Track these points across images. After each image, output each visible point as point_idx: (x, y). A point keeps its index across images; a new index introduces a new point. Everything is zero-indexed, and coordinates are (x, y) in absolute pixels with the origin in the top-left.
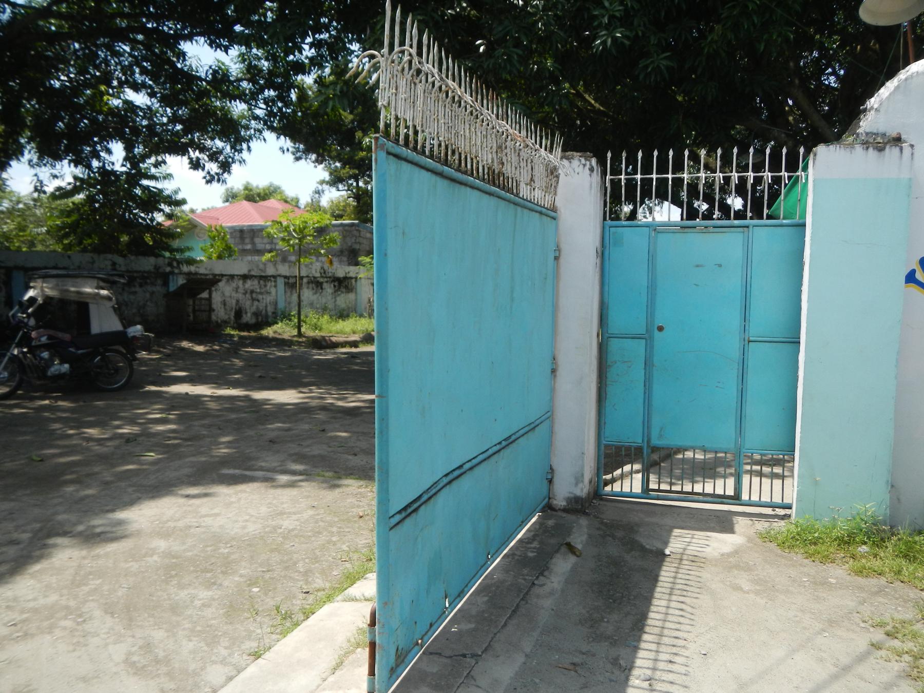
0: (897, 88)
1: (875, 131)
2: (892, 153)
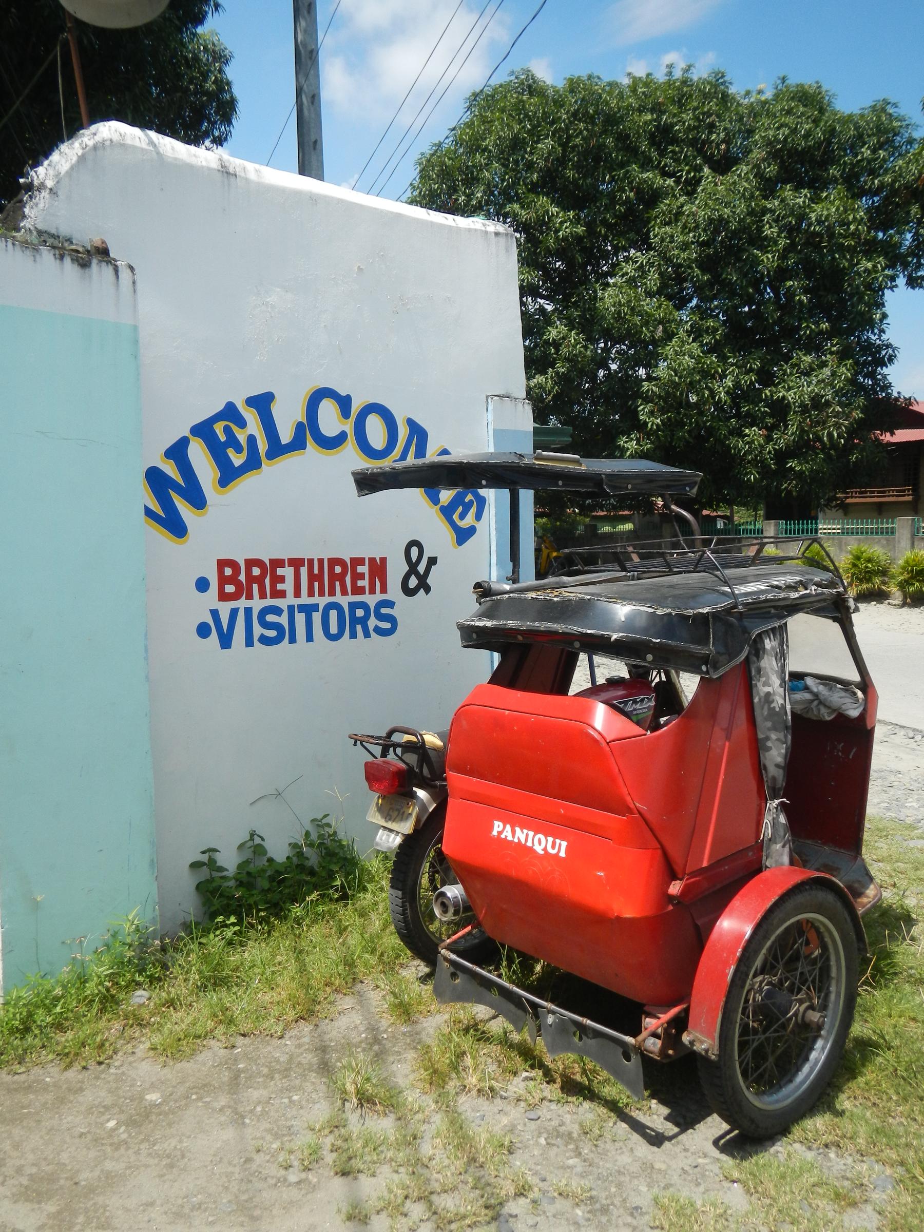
0: (82, 159)
1: (53, 231)
2: (99, 272)
